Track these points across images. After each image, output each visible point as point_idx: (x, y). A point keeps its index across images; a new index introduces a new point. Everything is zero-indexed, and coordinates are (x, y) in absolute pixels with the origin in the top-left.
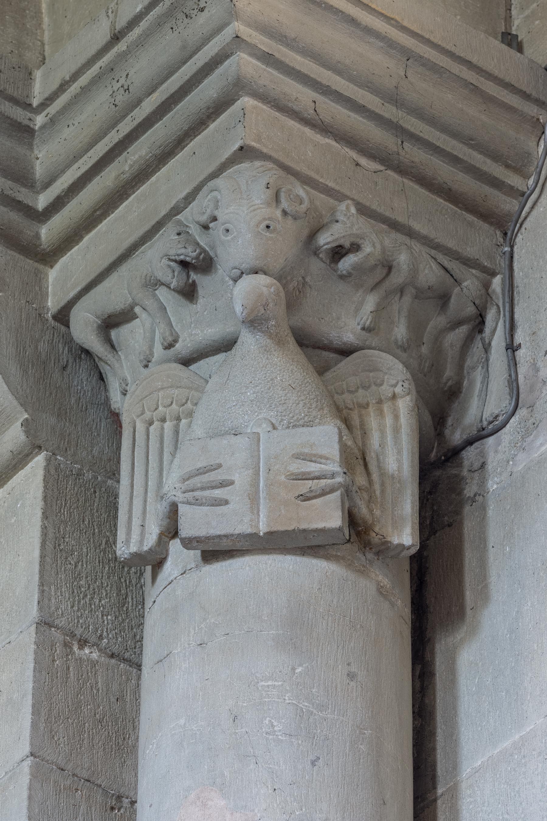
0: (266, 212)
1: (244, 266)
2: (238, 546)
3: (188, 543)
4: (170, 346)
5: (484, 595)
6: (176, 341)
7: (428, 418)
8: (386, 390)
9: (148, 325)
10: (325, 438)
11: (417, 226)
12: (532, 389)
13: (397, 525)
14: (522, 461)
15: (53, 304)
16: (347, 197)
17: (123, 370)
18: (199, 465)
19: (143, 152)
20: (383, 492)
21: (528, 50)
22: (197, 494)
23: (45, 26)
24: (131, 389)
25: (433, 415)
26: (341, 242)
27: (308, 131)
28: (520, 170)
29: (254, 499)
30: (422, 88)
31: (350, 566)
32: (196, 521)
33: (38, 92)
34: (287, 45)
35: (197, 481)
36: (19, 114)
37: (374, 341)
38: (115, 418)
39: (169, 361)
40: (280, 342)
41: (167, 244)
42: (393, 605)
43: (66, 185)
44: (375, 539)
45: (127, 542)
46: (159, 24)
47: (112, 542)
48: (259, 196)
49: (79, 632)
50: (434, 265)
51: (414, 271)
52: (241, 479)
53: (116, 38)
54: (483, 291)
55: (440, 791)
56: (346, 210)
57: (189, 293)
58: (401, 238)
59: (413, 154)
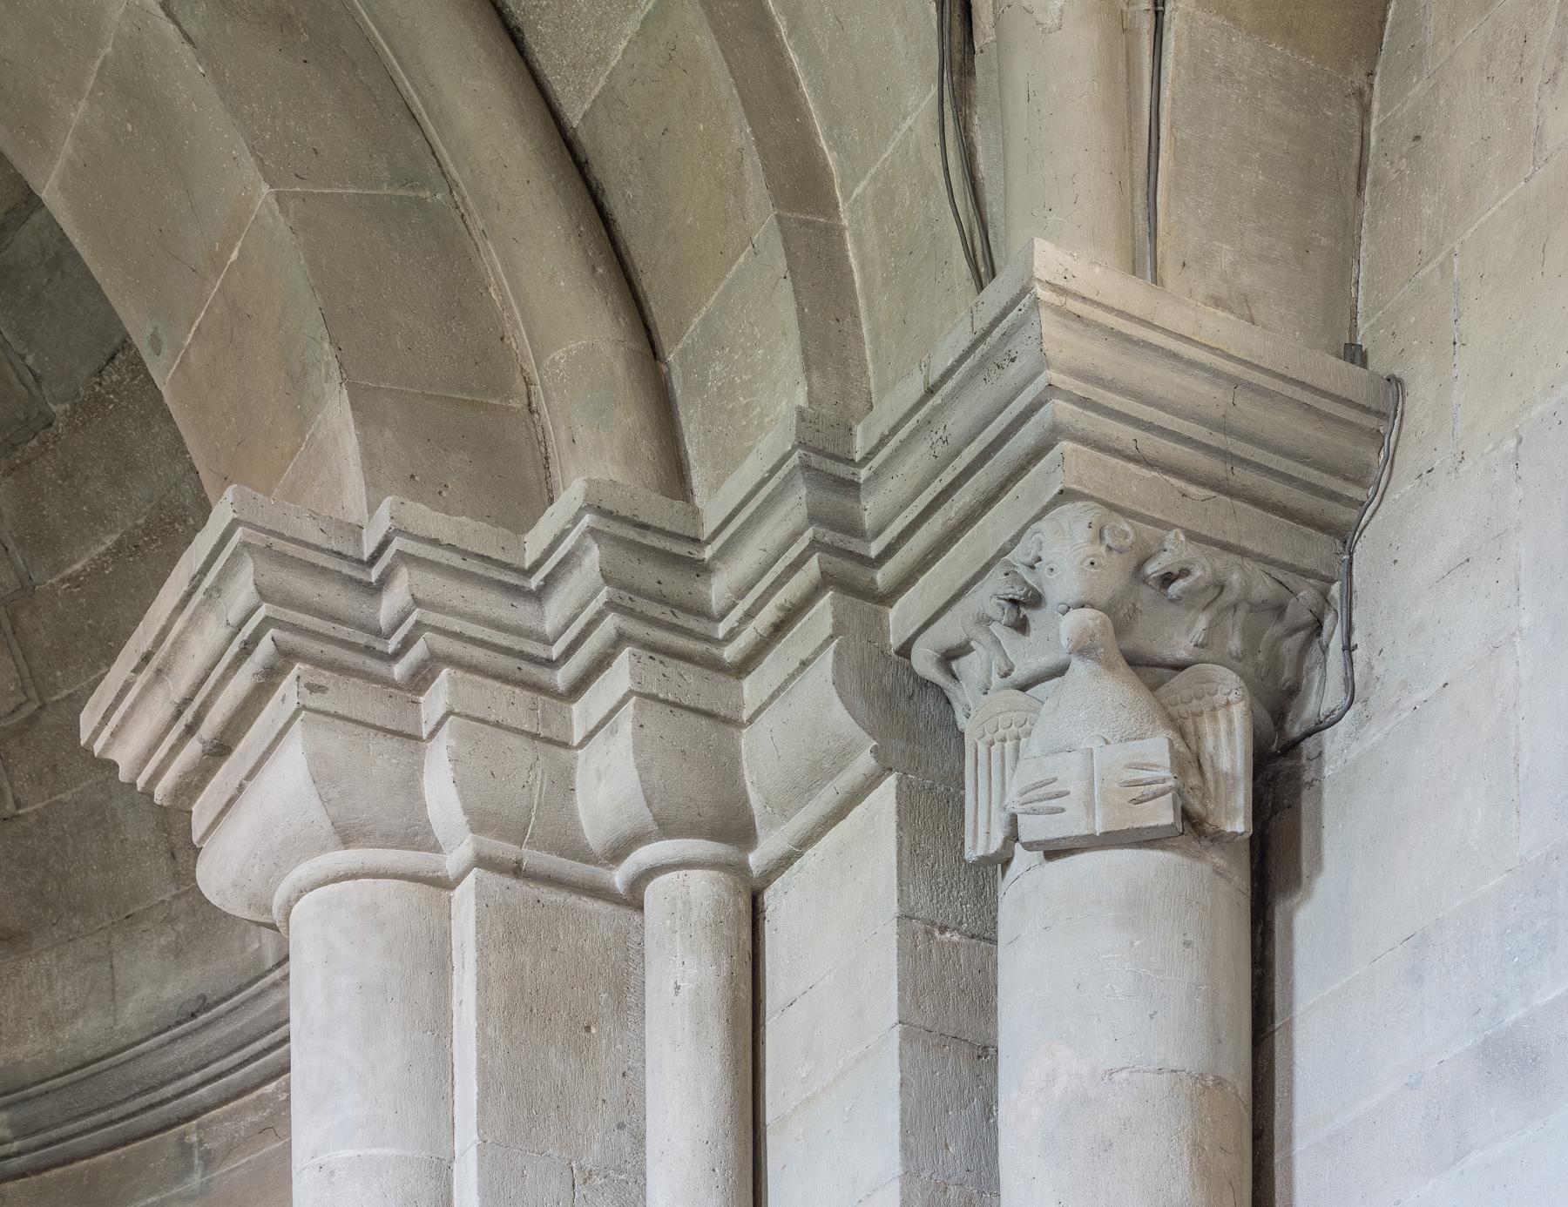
0: (1089, 549)
1: (1070, 601)
2: (1077, 845)
3: (1029, 846)
4: (1006, 675)
5: (1318, 865)
6: (1011, 670)
7: (1265, 716)
8: (1220, 699)
9: (984, 657)
10: (1157, 749)
11: (1248, 545)
12: (1366, 686)
13: (1230, 816)
14: (1356, 749)
15: (895, 641)
16: (1174, 526)
17: (964, 696)
18: (1036, 780)
19: (967, 499)
20: (1216, 788)
21: (1372, 361)
22: (1035, 805)
23: (870, 373)
24: (972, 713)
25: (1272, 713)
26: (1170, 569)
27: (1132, 466)
28: (1358, 481)
29: (1089, 806)
30: (1252, 414)
31: (1185, 853)
32: (1030, 829)
33: (859, 448)
34: (1105, 387)
35: (1034, 794)
36: (842, 470)
37: (1208, 655)
38: (961, 735)
39: (1007, 688)
40: (1110, 667)
41: (995, 586)
42: (1229, 881)
43: (895, 534)
44: (1209, 829)
45: (974, 847)
46: (972, 376)
47: (962, 851)
48: (1082, 534)
49: (939, 921)
50: (1268, 581)
51: (1247, 588)
52: (1076, 789)
53: (930, 392)
54: (1321, 599)
55: (1277, 1025)
56: (1174, 539)
57: (1021, 626)
58: (1233, 558)
59: (1244, 478)
